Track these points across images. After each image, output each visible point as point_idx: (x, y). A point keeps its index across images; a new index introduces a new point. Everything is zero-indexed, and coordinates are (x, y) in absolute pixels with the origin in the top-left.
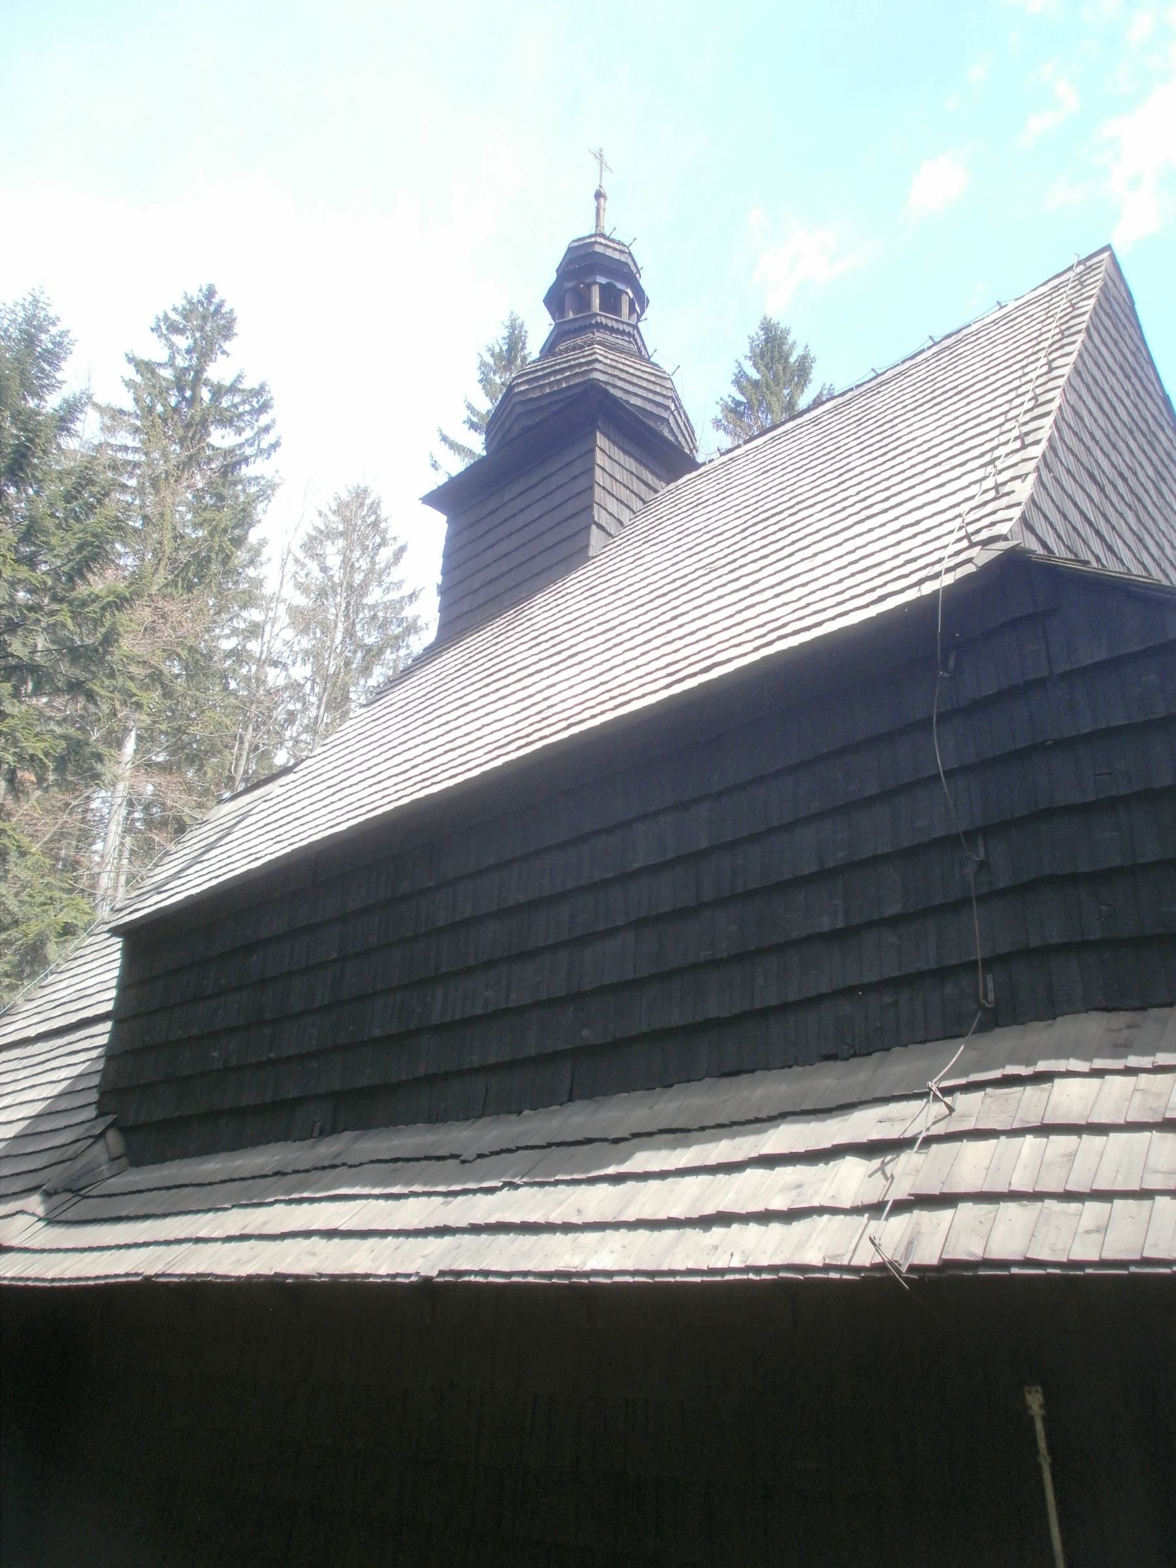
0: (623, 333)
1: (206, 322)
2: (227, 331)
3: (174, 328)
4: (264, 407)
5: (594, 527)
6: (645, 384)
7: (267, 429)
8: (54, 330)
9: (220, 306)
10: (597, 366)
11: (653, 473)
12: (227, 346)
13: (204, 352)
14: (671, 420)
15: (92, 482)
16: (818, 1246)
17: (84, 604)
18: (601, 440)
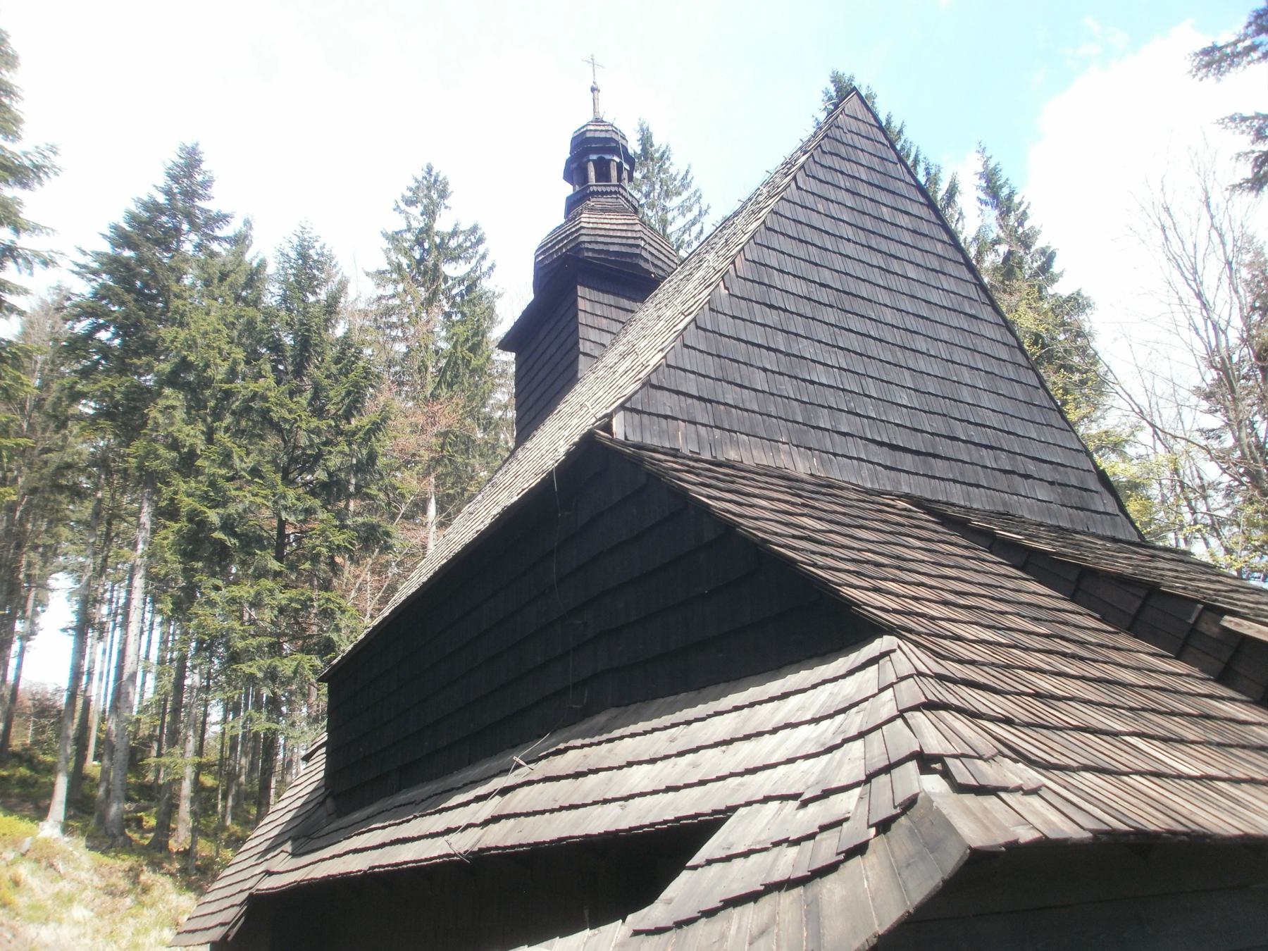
0: (611, 193)
1: (431, 192)
2: (443, 194)
3: (410, 203)
4: (480, 241)
5: (581, 357)
6: (619, 234)
7: (483, 257)
8: (317, 245)
9: (438, 175)
10: (583, 231)
11: (629, 299)
12: (447, 202)
13: (430, 213)
14: (644, 253)
15: (350, 346)
16: (462, 844)
17: (354, 433)
18: (581, 290)
